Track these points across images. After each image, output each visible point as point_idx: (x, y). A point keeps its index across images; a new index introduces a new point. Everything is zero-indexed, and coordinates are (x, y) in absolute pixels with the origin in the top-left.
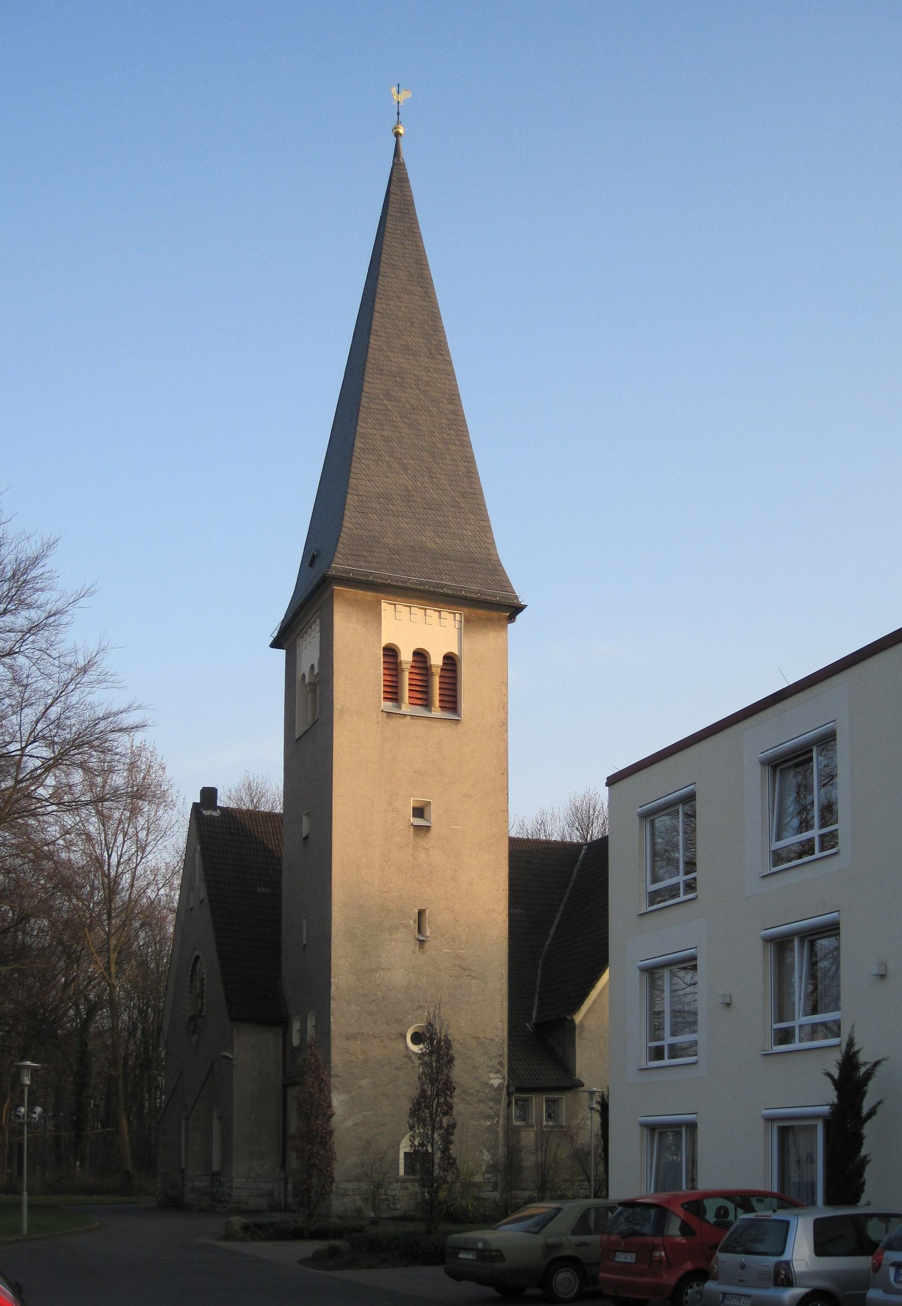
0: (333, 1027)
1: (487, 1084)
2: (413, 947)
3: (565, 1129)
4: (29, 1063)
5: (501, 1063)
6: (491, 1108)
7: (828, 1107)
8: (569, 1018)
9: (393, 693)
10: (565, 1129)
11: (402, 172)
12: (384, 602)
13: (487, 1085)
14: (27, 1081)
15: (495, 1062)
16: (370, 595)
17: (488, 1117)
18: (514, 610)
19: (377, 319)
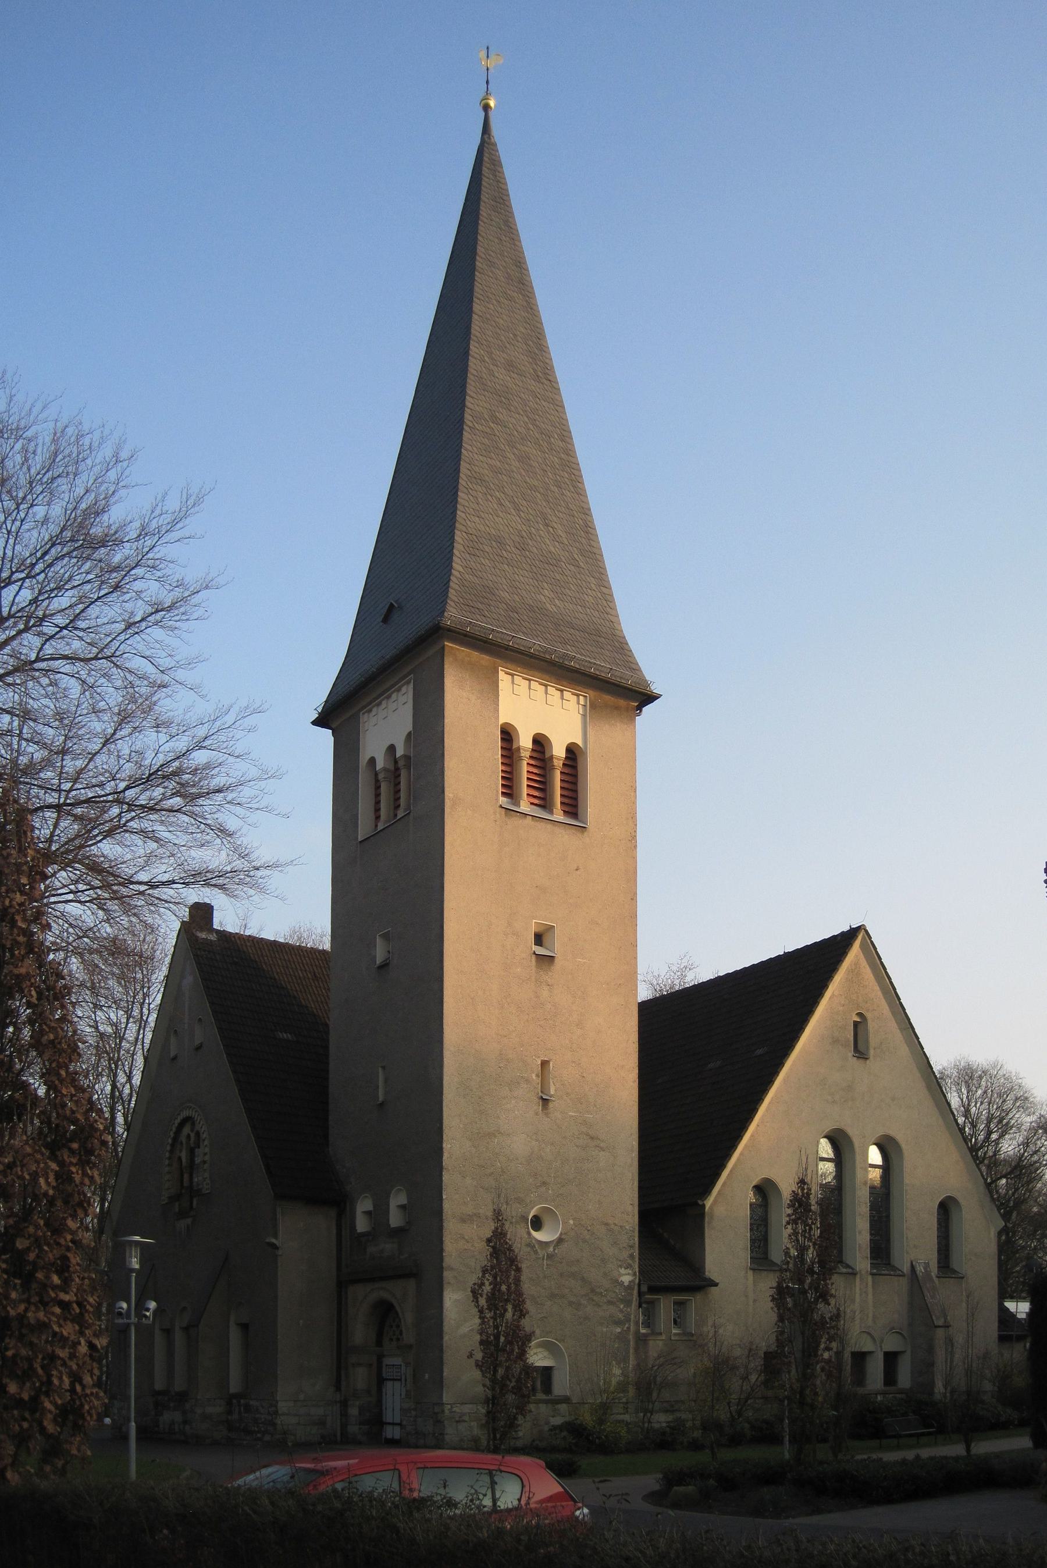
0: (446, 1206)
1: (617, 1281)
2: (536, 1107)
3: (695, 1338)
4: (137, 1238)
5: (631, 1256)
6: (621, 1311)
7: (1025, 1315)
8: (700, 1203)
9: (510, 789)
10: (695, 1338)
11: (493, 152)
12: (501, 670)
13: (617, 1282)
14: (135, 1263)
15: (625, 1254)
16: (485, 659)
17: (619, 1323)
18: (649, 698)
19: (477, 322)
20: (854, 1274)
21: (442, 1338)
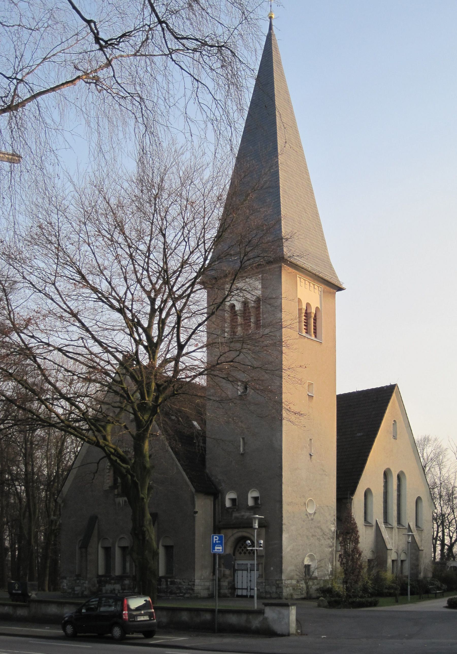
4: (257, 516)
5: (334, 519)
13: (330, 530)
20: (392, 528)
21: (282, 553)
